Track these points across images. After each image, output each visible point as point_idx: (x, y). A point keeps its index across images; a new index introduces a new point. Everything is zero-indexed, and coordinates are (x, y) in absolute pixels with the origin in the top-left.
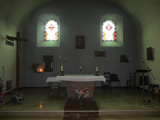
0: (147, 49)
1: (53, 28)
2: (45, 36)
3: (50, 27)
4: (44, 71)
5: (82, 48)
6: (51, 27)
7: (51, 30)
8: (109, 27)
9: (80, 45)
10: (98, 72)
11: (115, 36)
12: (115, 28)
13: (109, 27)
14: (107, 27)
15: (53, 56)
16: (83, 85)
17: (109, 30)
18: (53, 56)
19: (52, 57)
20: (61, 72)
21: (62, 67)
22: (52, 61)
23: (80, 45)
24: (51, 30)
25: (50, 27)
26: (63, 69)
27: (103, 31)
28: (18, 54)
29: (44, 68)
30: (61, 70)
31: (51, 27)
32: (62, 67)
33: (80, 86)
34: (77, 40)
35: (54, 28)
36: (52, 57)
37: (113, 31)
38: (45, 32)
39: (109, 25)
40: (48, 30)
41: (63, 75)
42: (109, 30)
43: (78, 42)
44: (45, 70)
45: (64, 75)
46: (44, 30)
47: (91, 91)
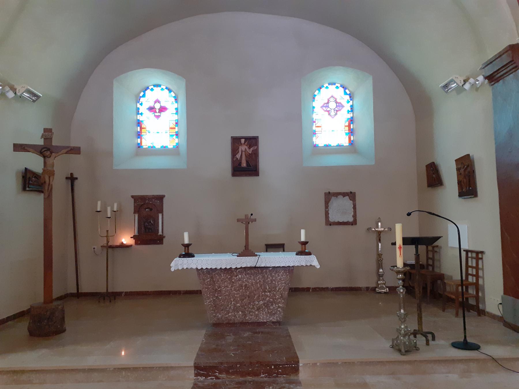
1: (163, 109)
2: (139, 135)
3: (151, 109)
4: (136, 243)
5: (250, 175)
6: (157, 106)
7: (158, 117)
9: (244, 164)
10: (305, 243)
13: (332, 105)
14: (326, 105)
15: (164, 196)
16: (252, 285)
17: (333, 113)
18: (164, 196)
19: (161, 198)
21: (303, 232)
22: (162, 212)
23: (244, 164)
24: (158, 117)
25: (151, 109)
27: (315, 117)
28: (76, 266)
29: (136, 234)
31: (157, 106)
32: (303, 232)
33: (246, 285)
34: (234, 151)
35: (167, 112)
36: (161, 198)
37: (344, 115)
39: (332, 99)
40: (147, 118)
41: (188, 255)
42: (333, 113)
43: (238, 156)
44: (139, 239)
45: (193, 256)
46: (136, 118)
47: (279, 303)
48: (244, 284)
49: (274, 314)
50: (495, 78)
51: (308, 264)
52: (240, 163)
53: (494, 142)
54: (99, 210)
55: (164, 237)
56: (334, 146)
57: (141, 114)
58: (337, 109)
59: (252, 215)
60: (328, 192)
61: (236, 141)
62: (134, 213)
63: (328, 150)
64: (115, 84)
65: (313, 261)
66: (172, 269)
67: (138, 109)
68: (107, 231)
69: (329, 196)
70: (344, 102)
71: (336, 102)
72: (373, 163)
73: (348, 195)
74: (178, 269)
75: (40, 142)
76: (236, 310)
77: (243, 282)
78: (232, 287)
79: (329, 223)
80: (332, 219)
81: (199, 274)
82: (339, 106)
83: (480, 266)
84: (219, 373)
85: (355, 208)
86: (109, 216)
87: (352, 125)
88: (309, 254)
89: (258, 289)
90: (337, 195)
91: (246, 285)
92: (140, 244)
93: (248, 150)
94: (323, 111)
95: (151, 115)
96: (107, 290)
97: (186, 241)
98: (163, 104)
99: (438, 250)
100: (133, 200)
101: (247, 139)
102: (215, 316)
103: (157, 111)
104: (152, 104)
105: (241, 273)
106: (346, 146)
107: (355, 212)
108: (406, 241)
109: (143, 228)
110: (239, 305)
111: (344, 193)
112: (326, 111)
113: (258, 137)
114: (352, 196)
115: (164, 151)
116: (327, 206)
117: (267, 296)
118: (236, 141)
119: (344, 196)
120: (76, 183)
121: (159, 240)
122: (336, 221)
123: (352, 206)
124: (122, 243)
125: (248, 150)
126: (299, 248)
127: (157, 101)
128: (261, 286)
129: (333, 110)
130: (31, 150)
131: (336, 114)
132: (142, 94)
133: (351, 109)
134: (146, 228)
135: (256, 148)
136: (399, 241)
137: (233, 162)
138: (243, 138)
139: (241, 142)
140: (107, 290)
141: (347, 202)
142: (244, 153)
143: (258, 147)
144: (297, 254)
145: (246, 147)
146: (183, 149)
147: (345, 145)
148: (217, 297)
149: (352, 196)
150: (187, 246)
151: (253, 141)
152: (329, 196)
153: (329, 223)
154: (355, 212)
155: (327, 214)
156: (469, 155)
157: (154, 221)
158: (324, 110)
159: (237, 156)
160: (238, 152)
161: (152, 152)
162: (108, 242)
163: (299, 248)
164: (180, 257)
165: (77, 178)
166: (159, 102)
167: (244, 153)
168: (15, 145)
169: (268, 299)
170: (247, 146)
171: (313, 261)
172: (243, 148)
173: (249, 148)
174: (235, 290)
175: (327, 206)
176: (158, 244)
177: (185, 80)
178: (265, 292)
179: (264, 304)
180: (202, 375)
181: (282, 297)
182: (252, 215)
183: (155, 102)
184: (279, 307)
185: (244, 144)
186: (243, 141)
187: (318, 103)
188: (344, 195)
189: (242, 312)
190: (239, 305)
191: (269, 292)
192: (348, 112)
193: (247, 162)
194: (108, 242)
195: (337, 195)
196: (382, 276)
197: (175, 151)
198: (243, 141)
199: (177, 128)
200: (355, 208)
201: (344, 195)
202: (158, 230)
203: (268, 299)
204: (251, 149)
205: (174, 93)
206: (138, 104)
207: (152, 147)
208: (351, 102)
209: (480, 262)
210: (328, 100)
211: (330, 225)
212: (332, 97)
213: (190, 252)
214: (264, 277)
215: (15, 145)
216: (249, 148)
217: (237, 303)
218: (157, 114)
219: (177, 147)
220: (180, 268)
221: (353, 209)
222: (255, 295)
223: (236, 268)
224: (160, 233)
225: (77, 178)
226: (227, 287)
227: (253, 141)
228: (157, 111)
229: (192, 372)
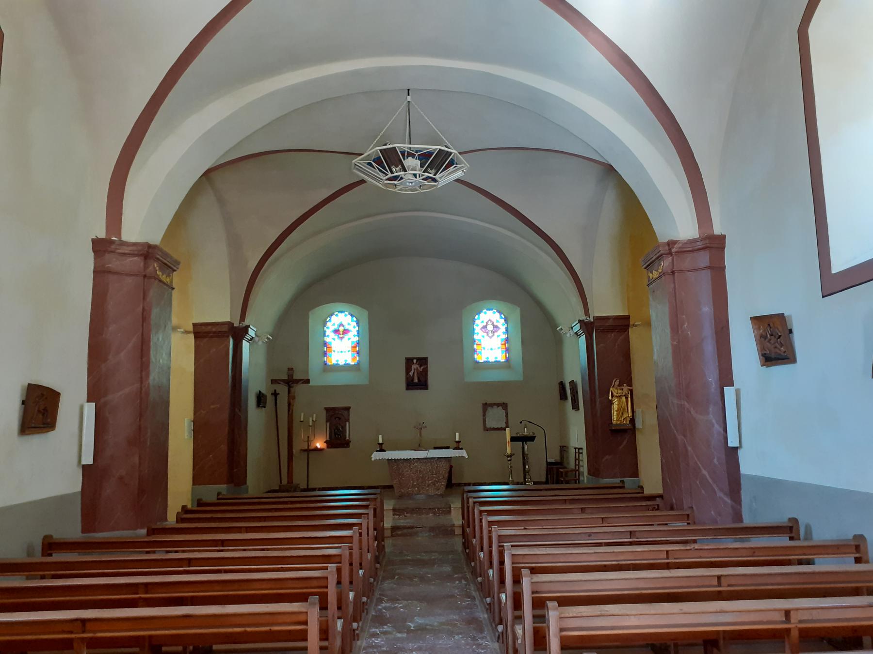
0: (569, 383)
1: (346, 332)
2: (325, 354)
3: (336, 332)
4: (328, 447)
5: (421, 389)
6: (341, 329)
8: (490, 327)
9: (416, 380)
10: (458, 442)
11: (507, 350)
12: (507, 329)
13: (490, 327)
15: (350, 408)
17: (490, 334)
18: (350, 408)
19: (348, 409)
20: (379, 444)
22: (348, 420)
23: (416, 380)
24: (341, 338)
25: (336, 332)
26: (459, 438)
27: (476, 337)
28: (290, 413)
30: (379, 441)
31: (341, 329)
33: (420, 470)
34: (408, 369)
37: (501, 335)
38: (325, 344)
39: (489, 323)
41: (382, 450)
42: (490, 334)
43: (411, 374)
44: (330, 444)
45: (385, 451)
48: (419, 470)
49: (438, 490)
50: (579, 334)
51: (461, 456)
52: (413, 380)
53: (580, 374)
54: (302, 420)
55: (350, 442)
56: (492, 362)
57: (328, 336)
58: (493, 331)
59: (423, 423)
60: (485, 403)
61: (409, 361)
62: (327, 421)
63: (487, 365)
64: (310, 313)
65: (463, 453)
66: (373, 459)
67: (325, 332)
68: (308, 437)
69: (486, 406)
70: (499, 325)
71: (493, 325)
72: (522, 379)
73: (501, 406)
74: (376, 460)
75: (286, 377)
76: (414, 486)
77: (418, 468)
78: (411, 471)
79: (486, 429)
80: (489, 425)
81: (389, 463)
82: (495, 329)
83: (581, 458)
84: (407, 514)
85: (507, 416)
86: (311, 425)
87: (507, 344)
88: (462, 449)
89: (428, 472)
90: (492, 405)
91: (420, 470)
92: (330, 448)
93: (419, 368)
94: (486, 321)
95: (336, 337)
96: (308, 486)
97: (381, 441)
98: (347, 327)
99: (566, 449)
100: (325, 412)
101: (419, 359)
102: (400, 491)
103: (341, 333)
104: (336, 327)
105: (417, 462)
106: (503, 362)
107: (507, 419)
108: (513, 439)
109: (333, 435)
110: (415, 483)
111: (498, 404)
112: (485, 332)
113: (428, 389)
114: (504, 406)
115: (347, 368)
116: (484, 415)
117: (434, 477)
118: (409, 361)
119: (498, 406)
120: (278, 397)
121: (346, 444)
122: (492, 427)
123: (505, 414)
124: (317, 447)
125: (419, 368)
126: (455, 445)
127: (341, 325)
128: (430, 471)
129: (490, 332)
130: (282, 383)
131: (494, 335)
132: (329, 319)
133: (506, 330)
134: (335, 434)
135: (425, 366)
136: (508, 439)
137: (407, 379)
138: (415, 358)
139: (413, 362)
140: (308, 486)
141: (500, 411)
142: (416, 371)
143: (427, 367)
144: (454, 449)
145: (418, 366)
146: (365, 365)
147: (501, 361)
148: (401, 478)
149: (504, 406)
150: (381, 444)
151: (423, 361)
152: (486, 406)
153: (486, 429)
154: (507, 419)
155: (484, 421)
156: (573, 381)
157: (342, 427)
158: (483, 331)
159: (410, 373)
160: (411, 370)
161: (337, 368)
162: (308, 446)
163: (455, 445)
164: (377, 451)
165: (279, 394)
166: (342, 325)
167: (416, 371)
168: (272, 380)
169: (434, 479)
170: (418, 365)
171: (463, 453)
172: (415, 367)
173: (420, 366)
174: (413, 473)
175: (484, 415)
176: (346, 447)
177: (367, 312)
178: (433, 474)
179: (432, 483)
180: (397, 515)
181: (444, 477)
182: (423, 423)
183: (340, 326)
184: (442, 485)
185: (416, 363)
186: (415, 361)
187: (477, 328)
188: (498, 405)
189: (418, 488)
190: (415, 483)
191: (436, 474)
192: (504, 333)
193: (419, 379)
194: (308, 446)
195: (492, 405)
196: (528, 472)
197: (357, 367)
198: (415, 361)
199: (358, 347)
200: (507, 416)
201: (498, 405)
202: (346, 436)
203: (434, 479)
204: (422, 368)
205: (356, 318)
206: (325, 328)
207: (337, 364)
208: (506, 324)
209: (580, 455)
210: (487, 323)
211: (487, 430)
212: (490, 320)
213: (383, 448)
214: (431, 464)
215: (272, 380)
216: (420, 366)
217: (414, 482)
218: (341, 336)
219: (358, 363)
220: (378, 459)
221: (505, 417)
222: (426, 477)
223: (414, 459)
224: (347, 438)
225: (279, 394)
226: (408, 471)
227: (423, 361)
228: (341, 333)
229: (391, 513)
